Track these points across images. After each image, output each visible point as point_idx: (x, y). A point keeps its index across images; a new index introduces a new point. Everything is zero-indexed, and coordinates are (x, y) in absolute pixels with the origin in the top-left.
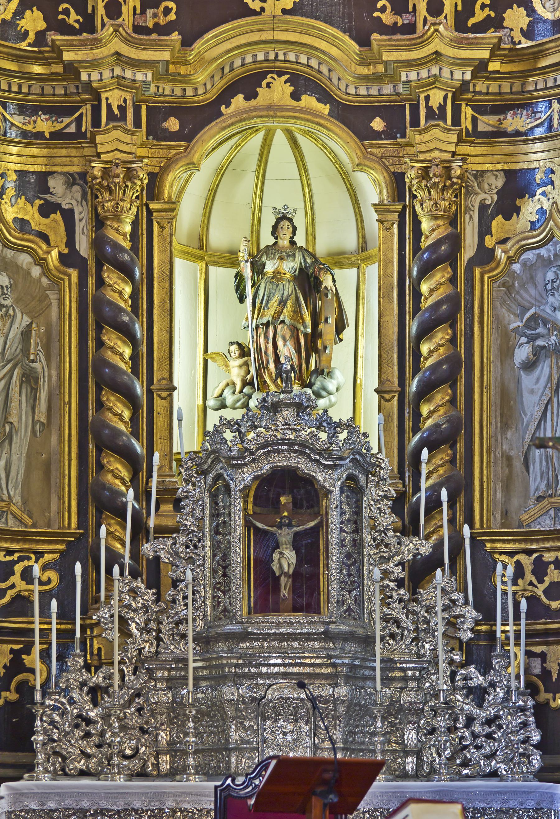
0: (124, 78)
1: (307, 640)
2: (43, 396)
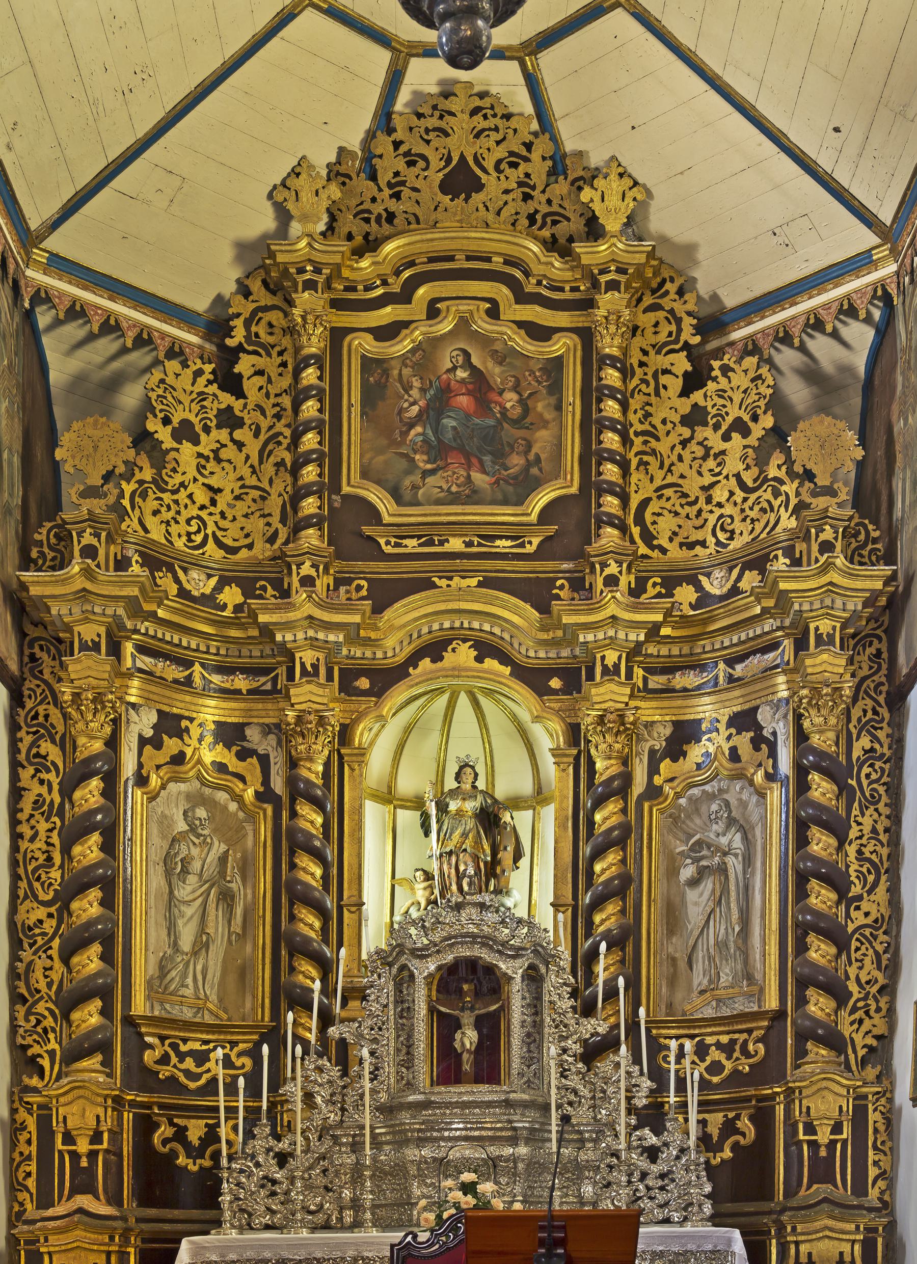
1: (488, 1107)
2: (239, 911)
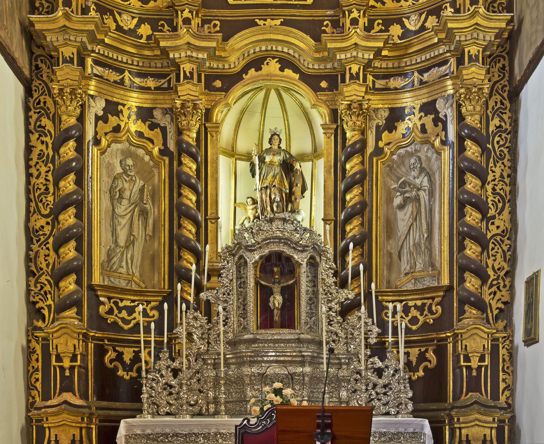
0: (192, 57)
1: (288, 343)
2: (151, 221)
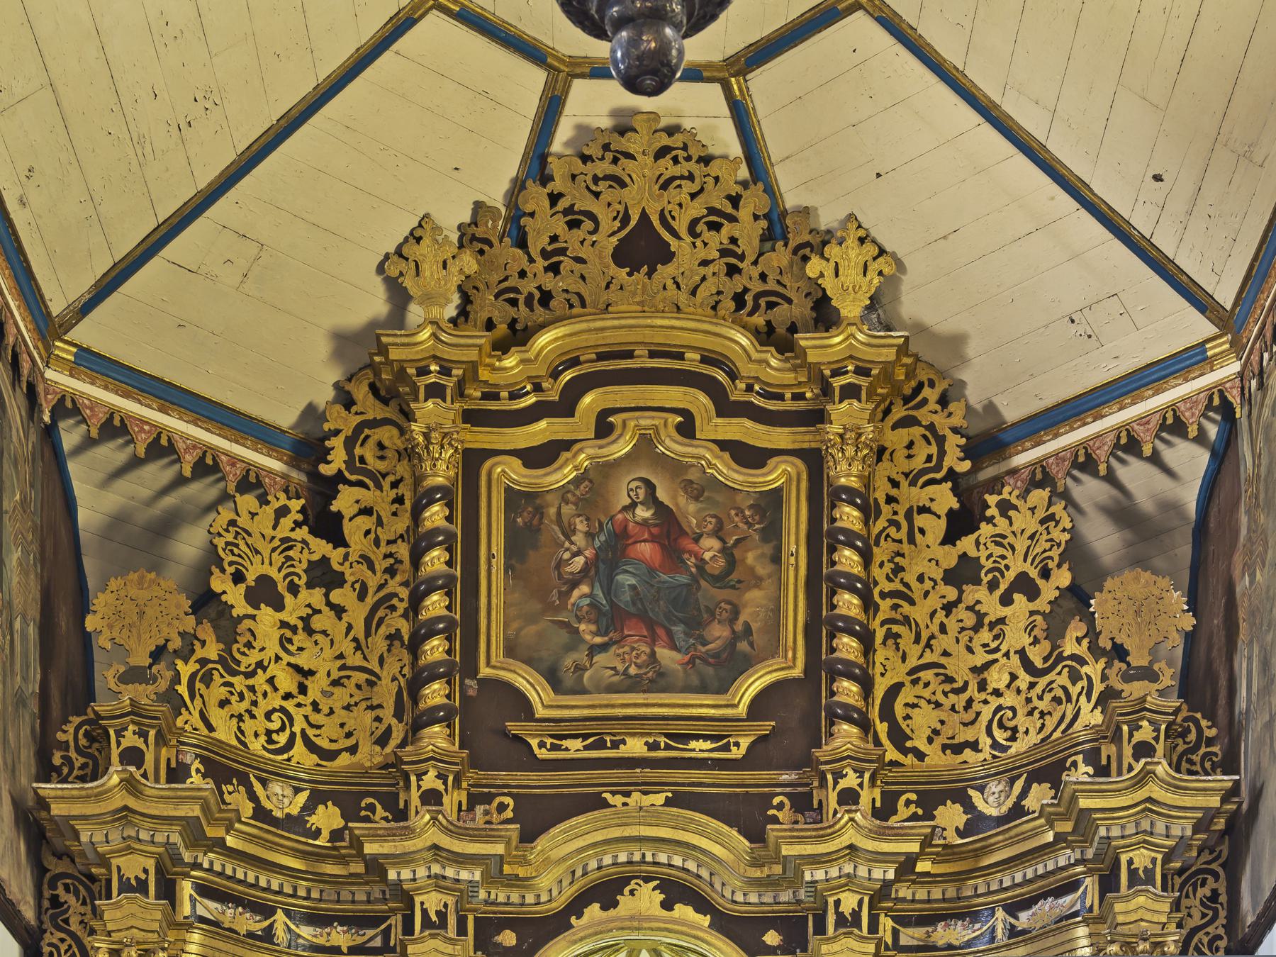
0: (444, 877)
